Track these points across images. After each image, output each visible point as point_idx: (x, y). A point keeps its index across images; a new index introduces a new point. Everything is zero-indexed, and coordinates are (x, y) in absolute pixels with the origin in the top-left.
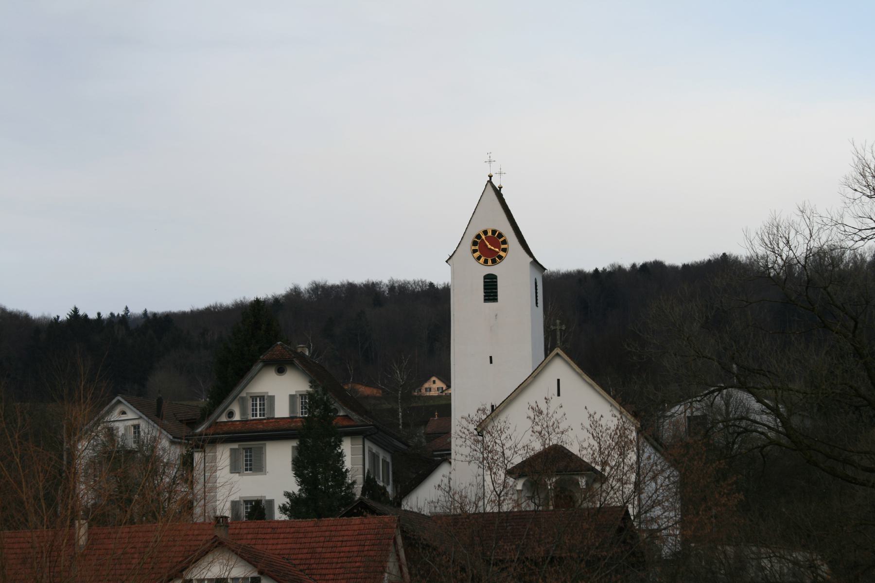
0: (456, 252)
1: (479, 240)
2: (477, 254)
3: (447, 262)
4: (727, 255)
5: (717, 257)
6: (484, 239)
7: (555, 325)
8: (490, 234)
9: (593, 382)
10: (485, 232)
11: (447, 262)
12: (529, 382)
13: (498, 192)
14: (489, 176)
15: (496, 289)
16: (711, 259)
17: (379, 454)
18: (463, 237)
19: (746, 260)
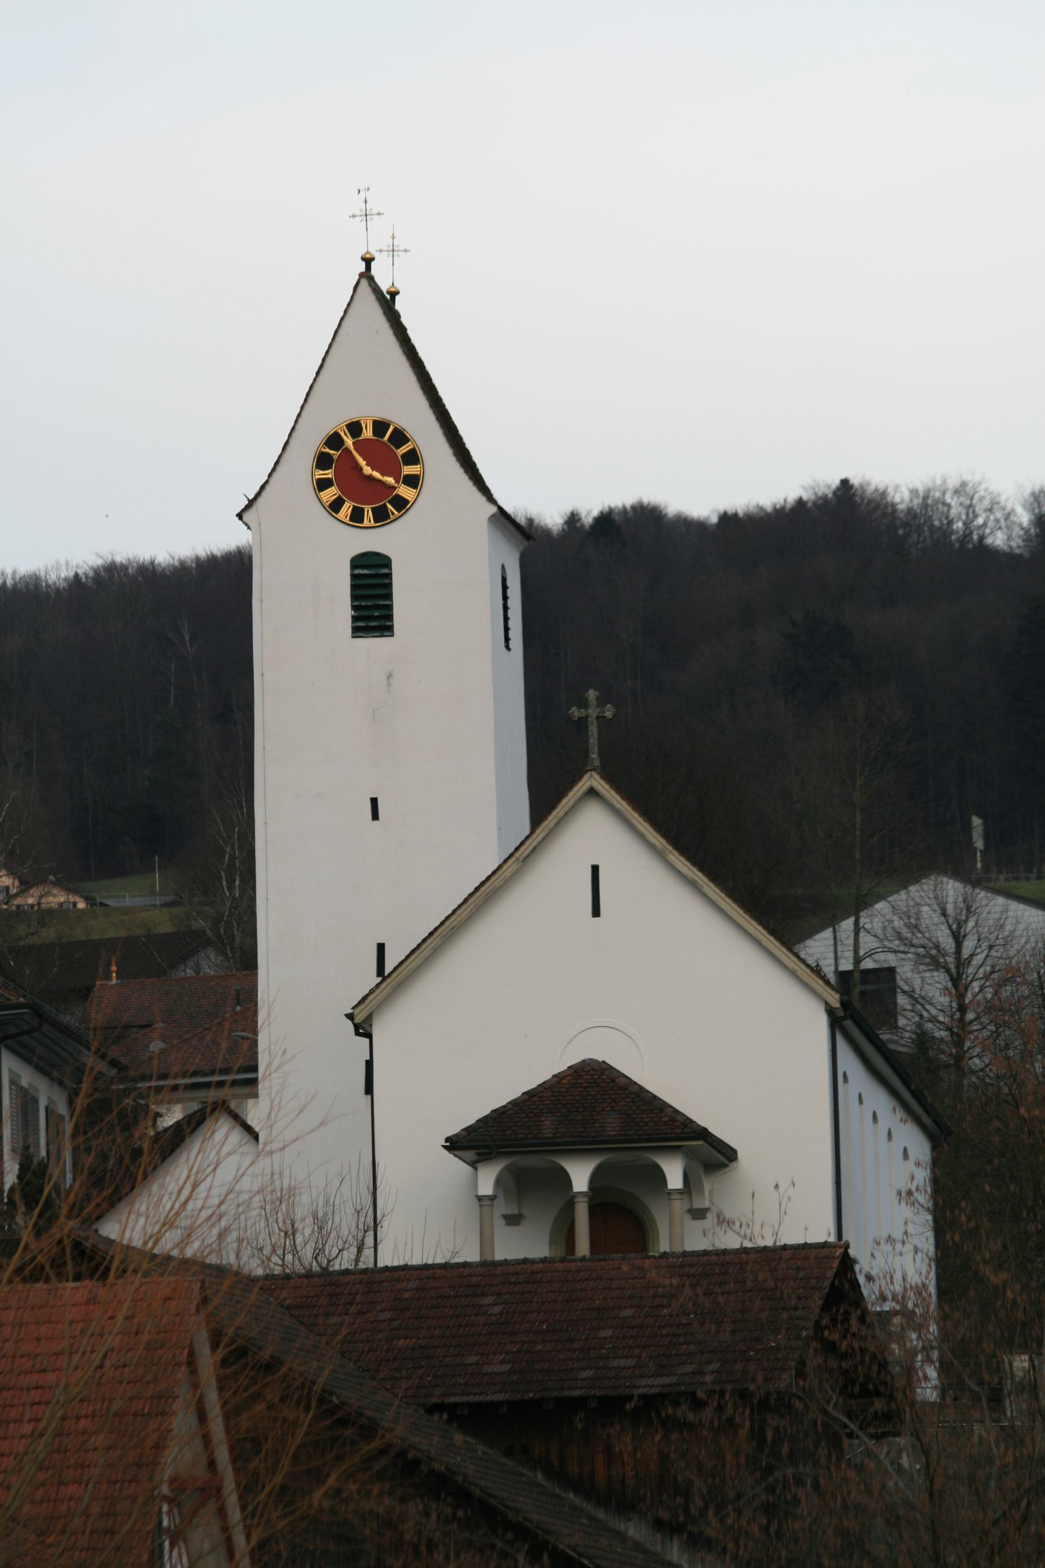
0: (268, 488)
1: (337, 450)
2: (331, 493)
3: (240, 516)
4: (852, 486)
5: (822, 490)
6: (352, 448)
7: (583, 704)
8: (368, 433)
9: (700, 875)
10: (355, 428)
11: (240, 516)
12: (508, 874)
13: (387, 303)
14: (363, 259)
15: (389, 596)
16: (805, 497)
17: (37, 1090)
18: (287, 443)
19: (911, 500)
